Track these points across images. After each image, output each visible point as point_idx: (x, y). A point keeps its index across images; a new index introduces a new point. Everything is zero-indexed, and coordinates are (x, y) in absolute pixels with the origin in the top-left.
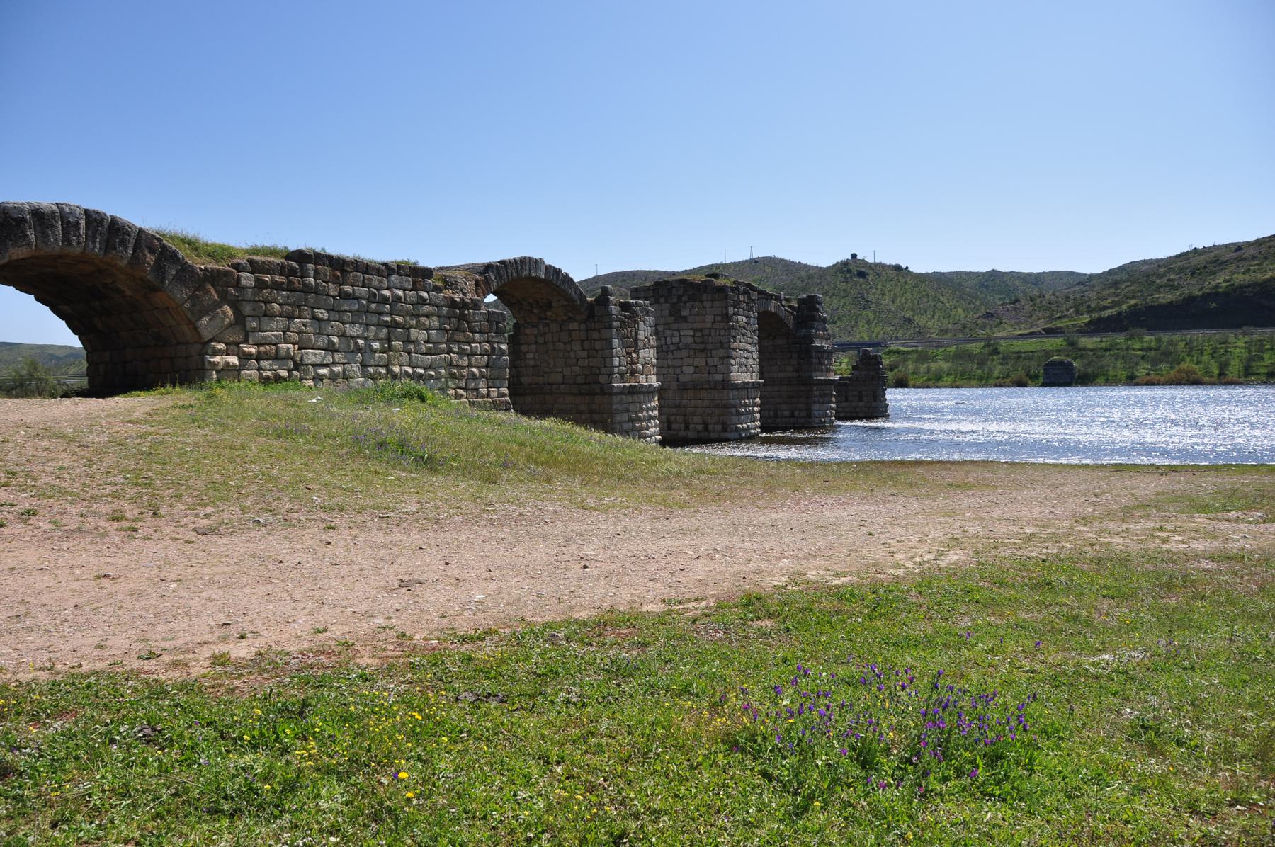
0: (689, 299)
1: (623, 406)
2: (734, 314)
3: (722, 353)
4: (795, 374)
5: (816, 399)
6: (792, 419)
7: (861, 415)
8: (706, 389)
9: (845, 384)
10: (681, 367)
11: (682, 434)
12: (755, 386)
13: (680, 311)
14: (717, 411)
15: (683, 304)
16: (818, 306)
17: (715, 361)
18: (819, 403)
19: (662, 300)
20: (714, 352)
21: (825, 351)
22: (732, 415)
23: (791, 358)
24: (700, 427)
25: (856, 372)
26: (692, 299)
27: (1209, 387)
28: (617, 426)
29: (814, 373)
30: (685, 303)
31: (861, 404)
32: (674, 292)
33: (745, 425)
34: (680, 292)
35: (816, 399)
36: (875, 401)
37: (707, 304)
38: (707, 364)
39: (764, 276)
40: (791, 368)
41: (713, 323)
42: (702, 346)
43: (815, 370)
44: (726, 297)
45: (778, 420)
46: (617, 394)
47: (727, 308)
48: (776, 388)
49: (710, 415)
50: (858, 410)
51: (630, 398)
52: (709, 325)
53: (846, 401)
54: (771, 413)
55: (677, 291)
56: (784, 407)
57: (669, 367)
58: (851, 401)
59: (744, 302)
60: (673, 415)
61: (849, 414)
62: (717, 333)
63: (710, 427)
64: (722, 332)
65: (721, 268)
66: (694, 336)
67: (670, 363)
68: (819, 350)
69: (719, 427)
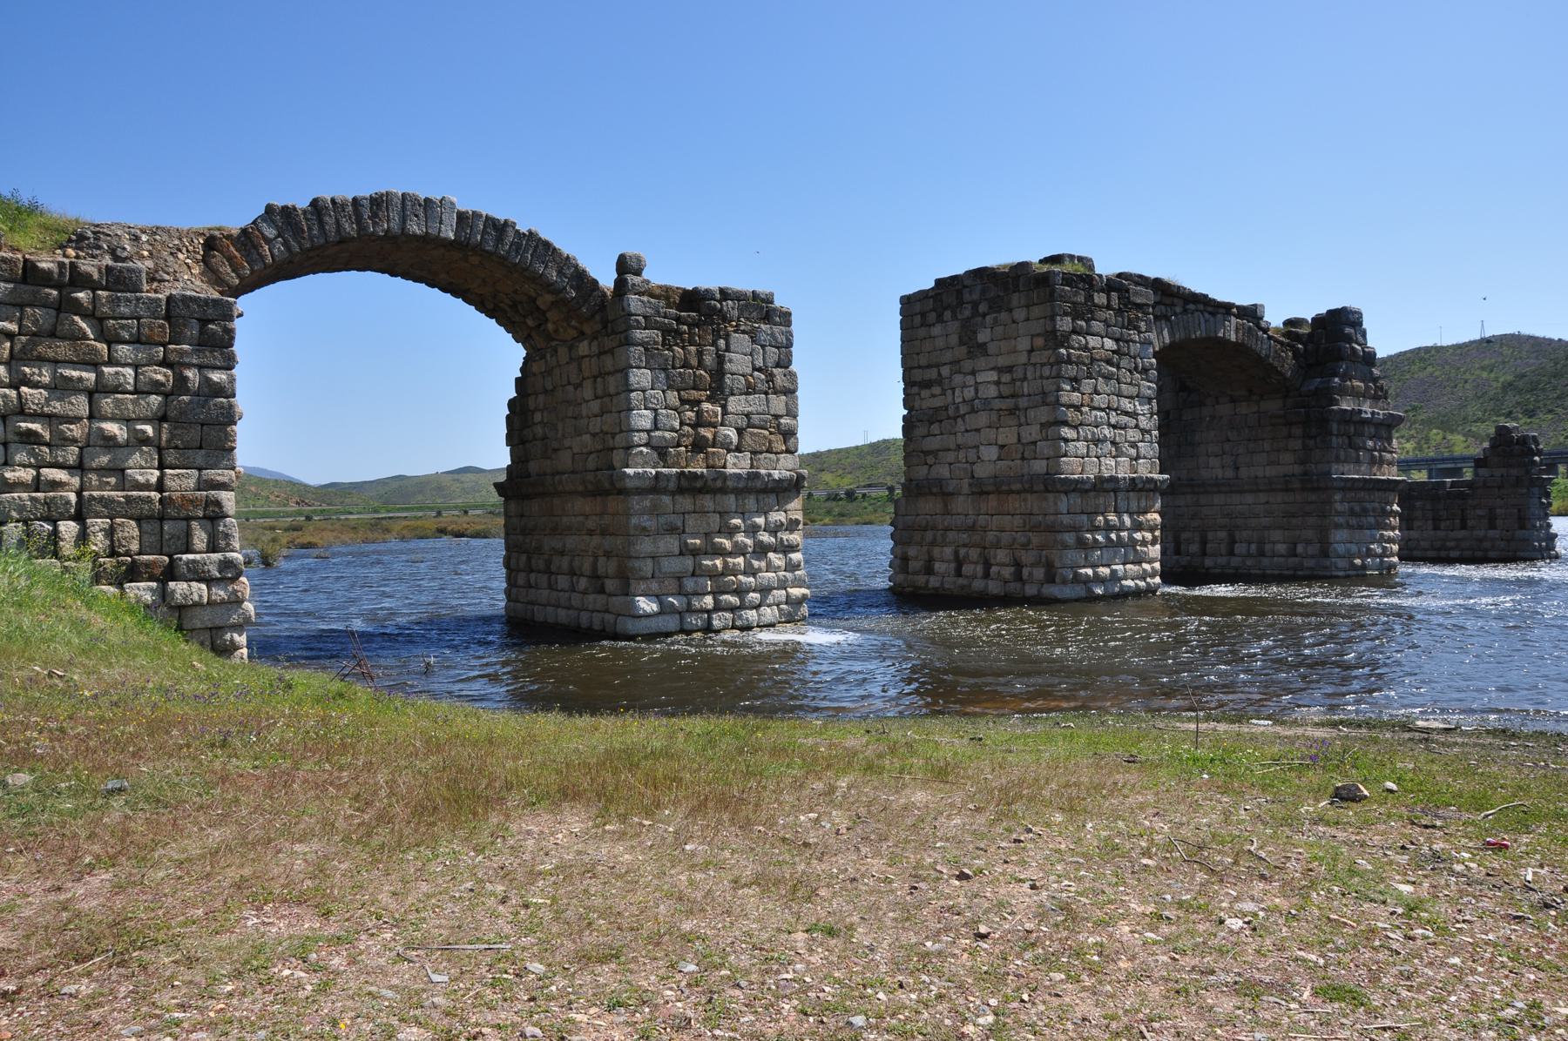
0: (990, 308)
1: (662, 520)
2: (1075, 331)
3: (1043, 414)
4: (1297, 469)
5: (1341, 520)
6: (1292, 560)
7: (1492, 554)
8: (1018, 492)
9: (1462, 496)
10: (977, 447)
11: (978, 585)
12: (1138, 487)
13: (975, 332)
14: (1036, 539)
15: (980, 319)
16: (1348, 330)
17: (1031, 433)
18: (1350, 527)
19: (948, 314)
20: (1031, 413)
21: (1365, 422)
22: (1066, 547)
23: (1290, 436)
24: (1007, 572)
25: (1482, 471)
26: (997, 306)
27: (1501, 565)
28: (647, 567)
29: (1335, 467)
30: (984, 315)
31: (1491, 533)
32: (967, 297)
33: (1104, 571)
34: (976, 296)
35: (1341, 520)
36: (1522, 527)
37: (1020, 314)
38: (1019, 440)
39: (1500, 360)
40: (1287, 457)
41: (1031, 351)
42: (1009, 403)
43: (1338, 460)
44: (1052, 296)
45: (1265, 561)
46: (641, 492)
47: (1052, 318)
48: (1263, 497)
49: (1025, 546)
50: (1487, 544)
51: (686, 502)
52: (1023, 358)
53: (1464, 527)
54: (1253, 547)
55: (970, 293)
56: (1277, 535)
57: (959, 447)
58: (1473, 528)
59: (1109, 307)
60: (965, 545)
61: (1468, 554)
62: (1038, 374)
63: (1025, 572)
64: (1046, 371)
65: (1433, 352)
66: (998, 383)
67: (960, 439)
68: (1352, 418)
69: (1039, 573)
